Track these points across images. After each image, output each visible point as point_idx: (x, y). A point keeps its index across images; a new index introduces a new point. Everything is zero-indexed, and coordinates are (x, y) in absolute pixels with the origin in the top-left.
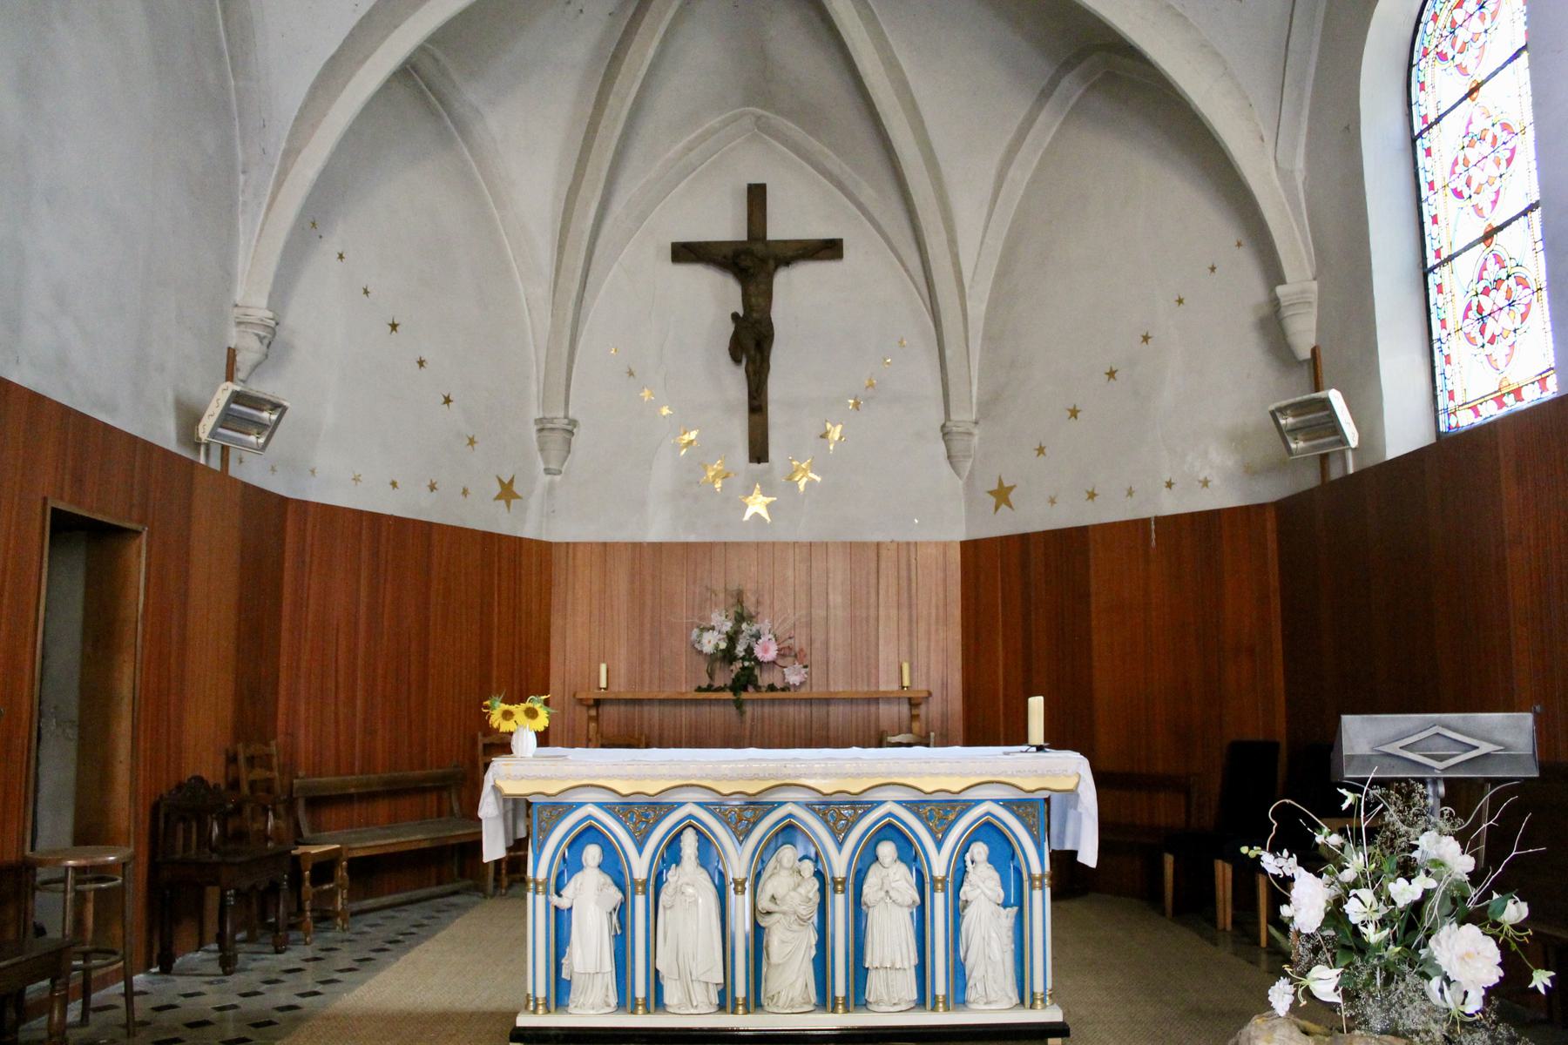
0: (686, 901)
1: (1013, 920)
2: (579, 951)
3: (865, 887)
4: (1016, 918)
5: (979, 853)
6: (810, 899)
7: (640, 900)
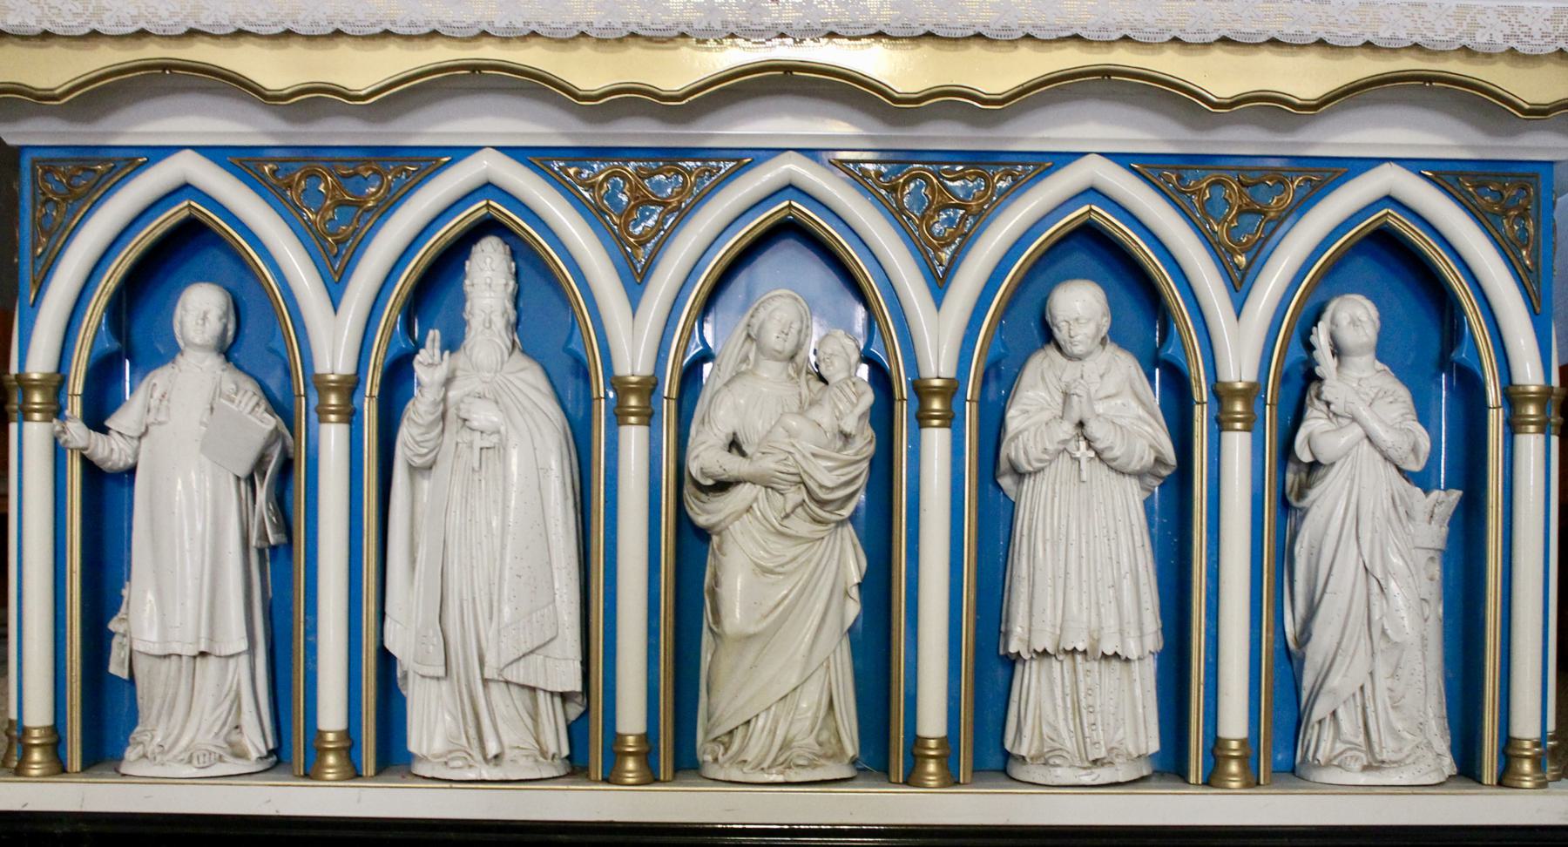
0: (471, 446)
1: (1445, 530)
2: (150, 597)
3: (1011, 413)
4: (1450, 524)
5: (1354, 322)
6: (846, 437)
7: (333, 439)
